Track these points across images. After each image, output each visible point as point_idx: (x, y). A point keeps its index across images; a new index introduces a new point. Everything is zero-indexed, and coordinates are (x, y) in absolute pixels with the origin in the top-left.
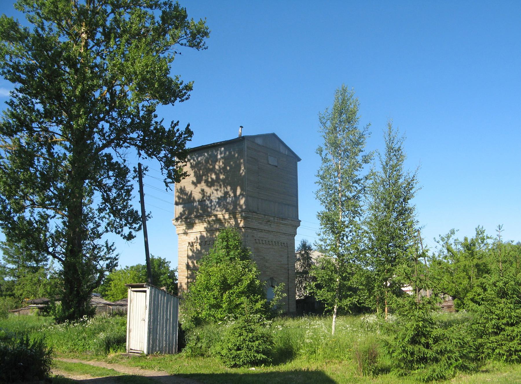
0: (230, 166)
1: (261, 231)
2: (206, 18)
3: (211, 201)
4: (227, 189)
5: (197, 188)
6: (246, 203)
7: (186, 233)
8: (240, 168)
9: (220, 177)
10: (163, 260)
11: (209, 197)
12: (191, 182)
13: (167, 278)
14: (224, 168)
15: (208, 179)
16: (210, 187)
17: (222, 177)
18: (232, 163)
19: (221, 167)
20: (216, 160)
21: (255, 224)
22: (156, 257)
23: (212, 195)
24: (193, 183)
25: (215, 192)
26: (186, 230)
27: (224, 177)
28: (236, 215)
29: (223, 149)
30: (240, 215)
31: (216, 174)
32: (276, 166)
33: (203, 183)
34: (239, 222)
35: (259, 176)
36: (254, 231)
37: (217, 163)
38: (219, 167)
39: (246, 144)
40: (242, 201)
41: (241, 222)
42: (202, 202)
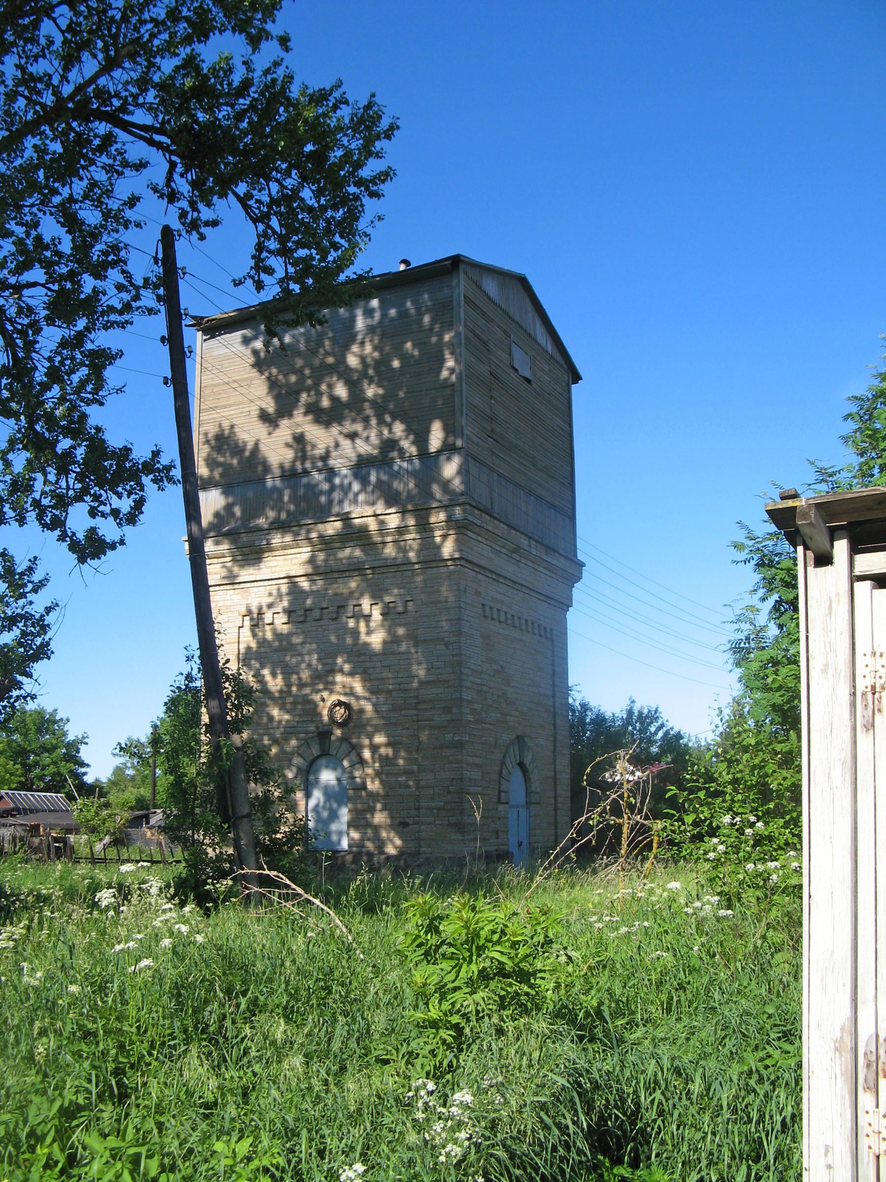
0: (405, 358)
1: (497, 577)
3: (331, 473)
5: (278, 433)
6: (463, 471)
8: (442, 361)
9: (362, 391)
10: (51, 715)
11: (325, 457)
12: (255, 413)
13: (61, 761)
14: (382, 364)
15: (318, 401)
16: (327, 424)
17: (371, 391)
18: (409, 345)
19: (369, 360)
20: (347, 337)
21: (482, 553)
23: (334, 454)
24: (264, 416)
25: (346, 444)
26: (236, 569)
27: (381, 391)
28: (428, 517)
29: (375, 303)
30: (442, 516)
32: (528, 381)
34: (438, 540)
35: (492, 397)
36: (480, 576)
37: (355, 348)
38: (363, 359)
39: (461, 285)
40: (450, 469)
41: (443, 541)
42: (290, 475)
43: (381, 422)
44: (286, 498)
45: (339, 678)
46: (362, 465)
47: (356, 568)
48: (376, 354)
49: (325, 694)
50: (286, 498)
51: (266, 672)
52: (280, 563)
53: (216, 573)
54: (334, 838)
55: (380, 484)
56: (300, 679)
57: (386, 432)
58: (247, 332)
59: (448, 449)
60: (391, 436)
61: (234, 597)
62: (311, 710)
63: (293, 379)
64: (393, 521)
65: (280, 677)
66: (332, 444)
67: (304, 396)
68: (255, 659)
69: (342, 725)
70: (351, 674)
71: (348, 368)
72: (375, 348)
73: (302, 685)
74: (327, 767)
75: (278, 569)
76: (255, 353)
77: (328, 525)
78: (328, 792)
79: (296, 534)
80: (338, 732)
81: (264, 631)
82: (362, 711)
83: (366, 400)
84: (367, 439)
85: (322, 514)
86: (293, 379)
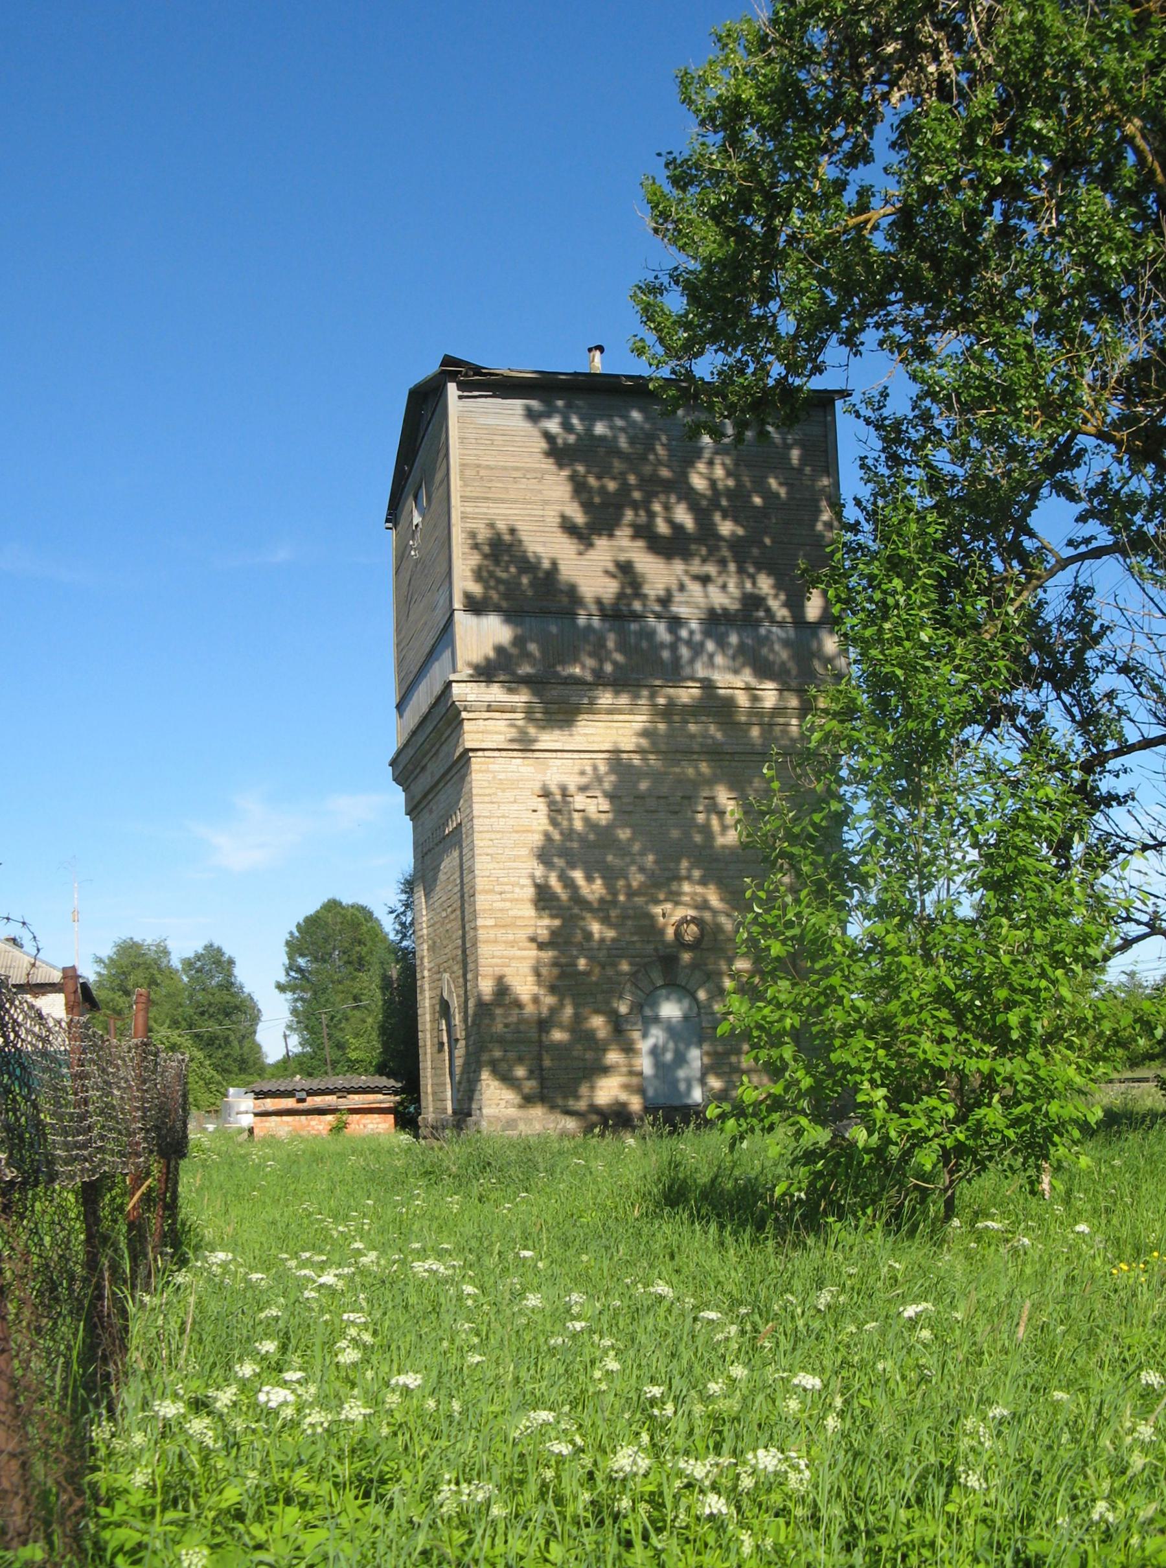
2: (659, 155)
3: (675, 622)
4: (754, 584)
5: (592, 554)
7: (524, 745)
8: (818, 512)
11: (666, 600)
22: (149, 941)
23: (678, 597)
24: (568, 527)
25: (695, 588)
26: (532, 731)
27: (740, 531)
31: (695, 508)
33: (623, 535)
37: (701, 467)
38: (713, 483)
43: (741, 571)
44: (611, 644)
45: (686, 887)
46: (715, 621)
47: (714, 753)
48: (731, 483)
49: (668, 906)
50: (611, 644)
51: (578, 875)
52: (602, 731)
53: (500, 733)
54: (682, 1086)
55: (742, 649)
56: (629, 886)
57: (748, 585)
58: (534, 404)
59: (829, 621)
60: (756, 591)
61: (522, 769)
62: (650, 928)
63: (612, 486)
64: (770, 696)
65: (599, 882)
66: (674, 587)
67: (629, 515)
68: (560, 856)
69: (694, 946)
70: (703, 882)
71: (691, 489)
72: (729, 474)
73: (631, 894)
74: (668, 999)
75: (596, 739)
76: (548, 436)
77: (682, 691)
78: (671, 1030)
79: (637, 696)
80: (686, 957)
81: (570, 820)
82: (719, 928)
83: (720, 538)
84: (724, 587)
85: (675, 673)
86: (612, 486)
